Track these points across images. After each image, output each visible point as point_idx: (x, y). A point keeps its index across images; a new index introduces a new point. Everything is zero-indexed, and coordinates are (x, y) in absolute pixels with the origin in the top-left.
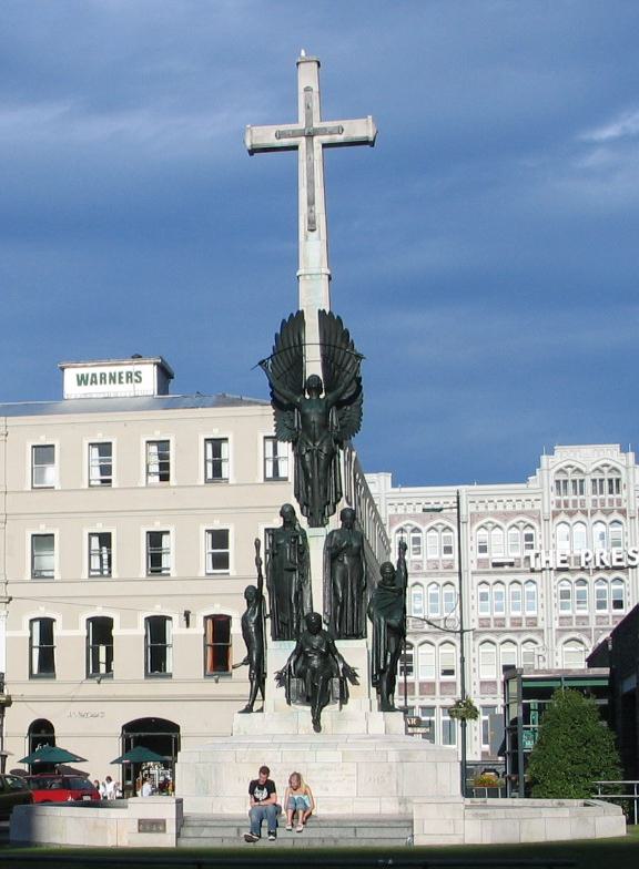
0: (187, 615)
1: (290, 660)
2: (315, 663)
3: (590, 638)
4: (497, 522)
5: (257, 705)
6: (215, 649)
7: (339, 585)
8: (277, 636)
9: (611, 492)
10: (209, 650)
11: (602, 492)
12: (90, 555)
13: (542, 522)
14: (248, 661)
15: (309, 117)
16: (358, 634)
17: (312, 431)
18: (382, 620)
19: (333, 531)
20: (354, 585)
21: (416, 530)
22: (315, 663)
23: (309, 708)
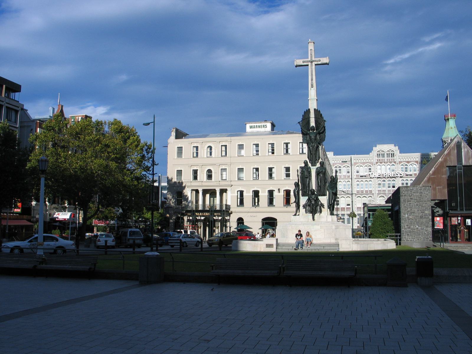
0: (279, 190)
1: (306, 202)
2: (313, 202)
3: (386, 196)
4: (361, 165)
5: (298, 214)
6: (286, 198)
7: (319, 182)
8: (303, 195)
9: (392, 157)
10: (285, 199)
11: (389, 157)
12: (253, 174)
13: (373, 165)
14: (295, 202)
15: (311, 57)
16: (324, 195)
17: (312, 141)
18: (331, 191)
19: (318, 167)
20: (323, 182)
21: (340, 167)
22: (313, 202)
23: (311, 215)
